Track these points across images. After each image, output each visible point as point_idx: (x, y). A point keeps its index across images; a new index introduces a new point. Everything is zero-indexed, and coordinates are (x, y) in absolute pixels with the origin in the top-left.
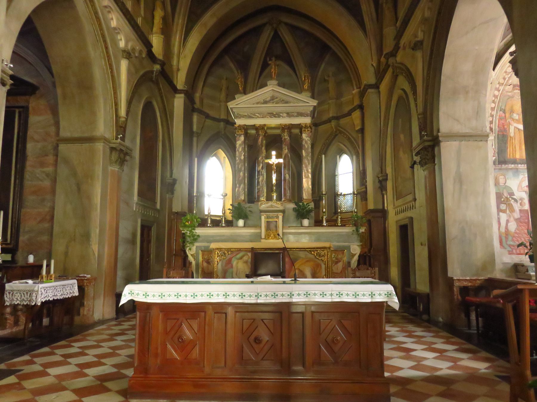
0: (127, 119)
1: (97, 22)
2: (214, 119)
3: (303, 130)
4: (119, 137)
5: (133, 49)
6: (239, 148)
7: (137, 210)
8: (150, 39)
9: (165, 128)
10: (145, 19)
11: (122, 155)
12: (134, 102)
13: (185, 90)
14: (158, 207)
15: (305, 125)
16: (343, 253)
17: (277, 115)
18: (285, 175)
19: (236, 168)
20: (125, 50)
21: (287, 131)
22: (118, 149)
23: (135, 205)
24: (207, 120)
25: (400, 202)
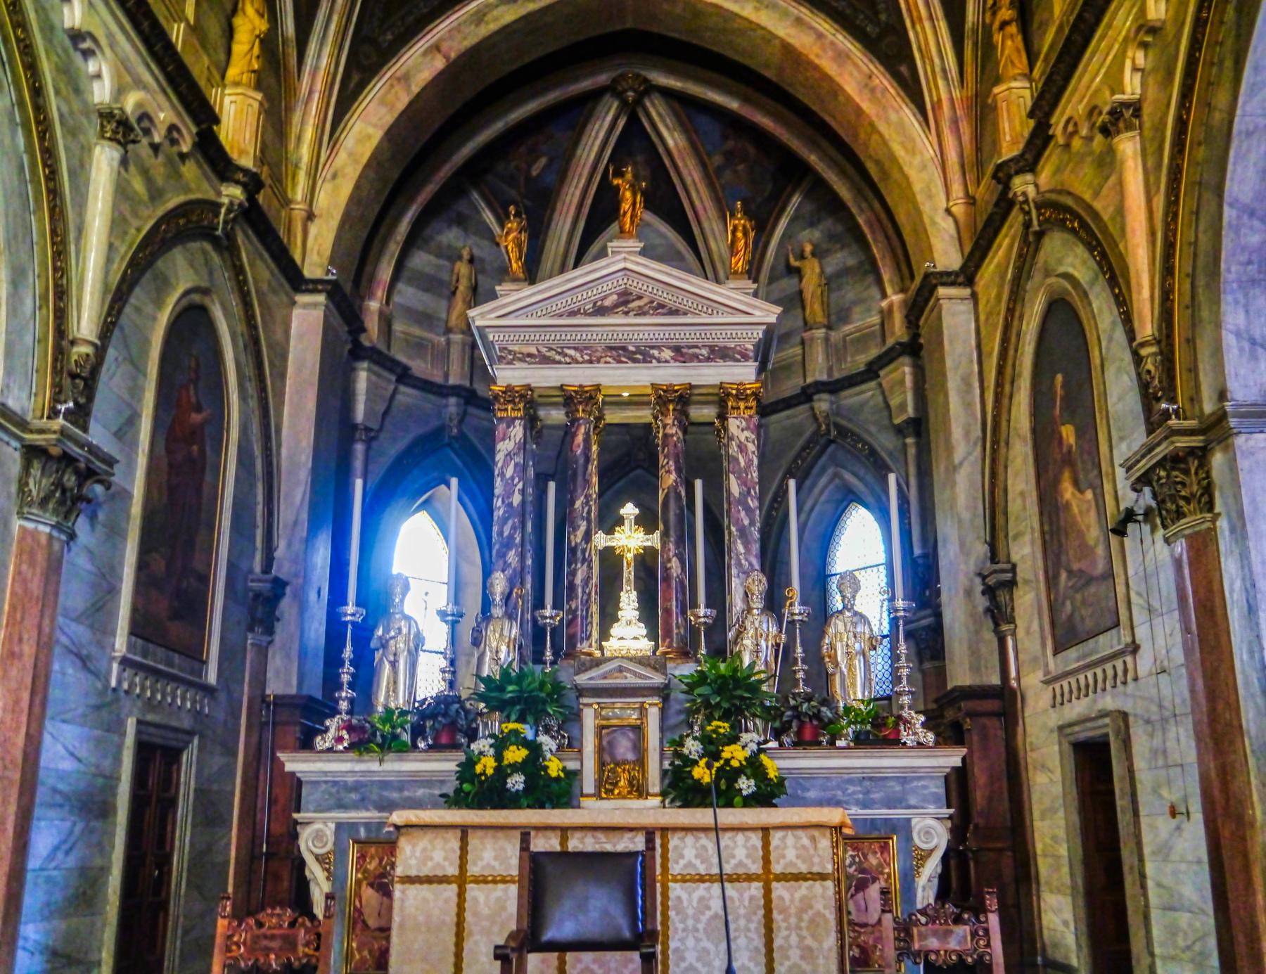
0: (101, 351)
2: (426, 386)
3: (730, 404)
4: (62, 408)
5: (145, 117)
6: (506, 464)
7: (125, 686)
9: (253, 403)
10: (196, 30)
11: (70, 480)
12: (138, 296)
13: (328, 282)
14: (212, 677)
15: (737, 389)
16: (884, 848)
17: (641, 355)
19: (495, 535)
21: (674, 410)
22: (55, 451)
23: (115, 666)
24: (402, 388)
25: (1072, 657)
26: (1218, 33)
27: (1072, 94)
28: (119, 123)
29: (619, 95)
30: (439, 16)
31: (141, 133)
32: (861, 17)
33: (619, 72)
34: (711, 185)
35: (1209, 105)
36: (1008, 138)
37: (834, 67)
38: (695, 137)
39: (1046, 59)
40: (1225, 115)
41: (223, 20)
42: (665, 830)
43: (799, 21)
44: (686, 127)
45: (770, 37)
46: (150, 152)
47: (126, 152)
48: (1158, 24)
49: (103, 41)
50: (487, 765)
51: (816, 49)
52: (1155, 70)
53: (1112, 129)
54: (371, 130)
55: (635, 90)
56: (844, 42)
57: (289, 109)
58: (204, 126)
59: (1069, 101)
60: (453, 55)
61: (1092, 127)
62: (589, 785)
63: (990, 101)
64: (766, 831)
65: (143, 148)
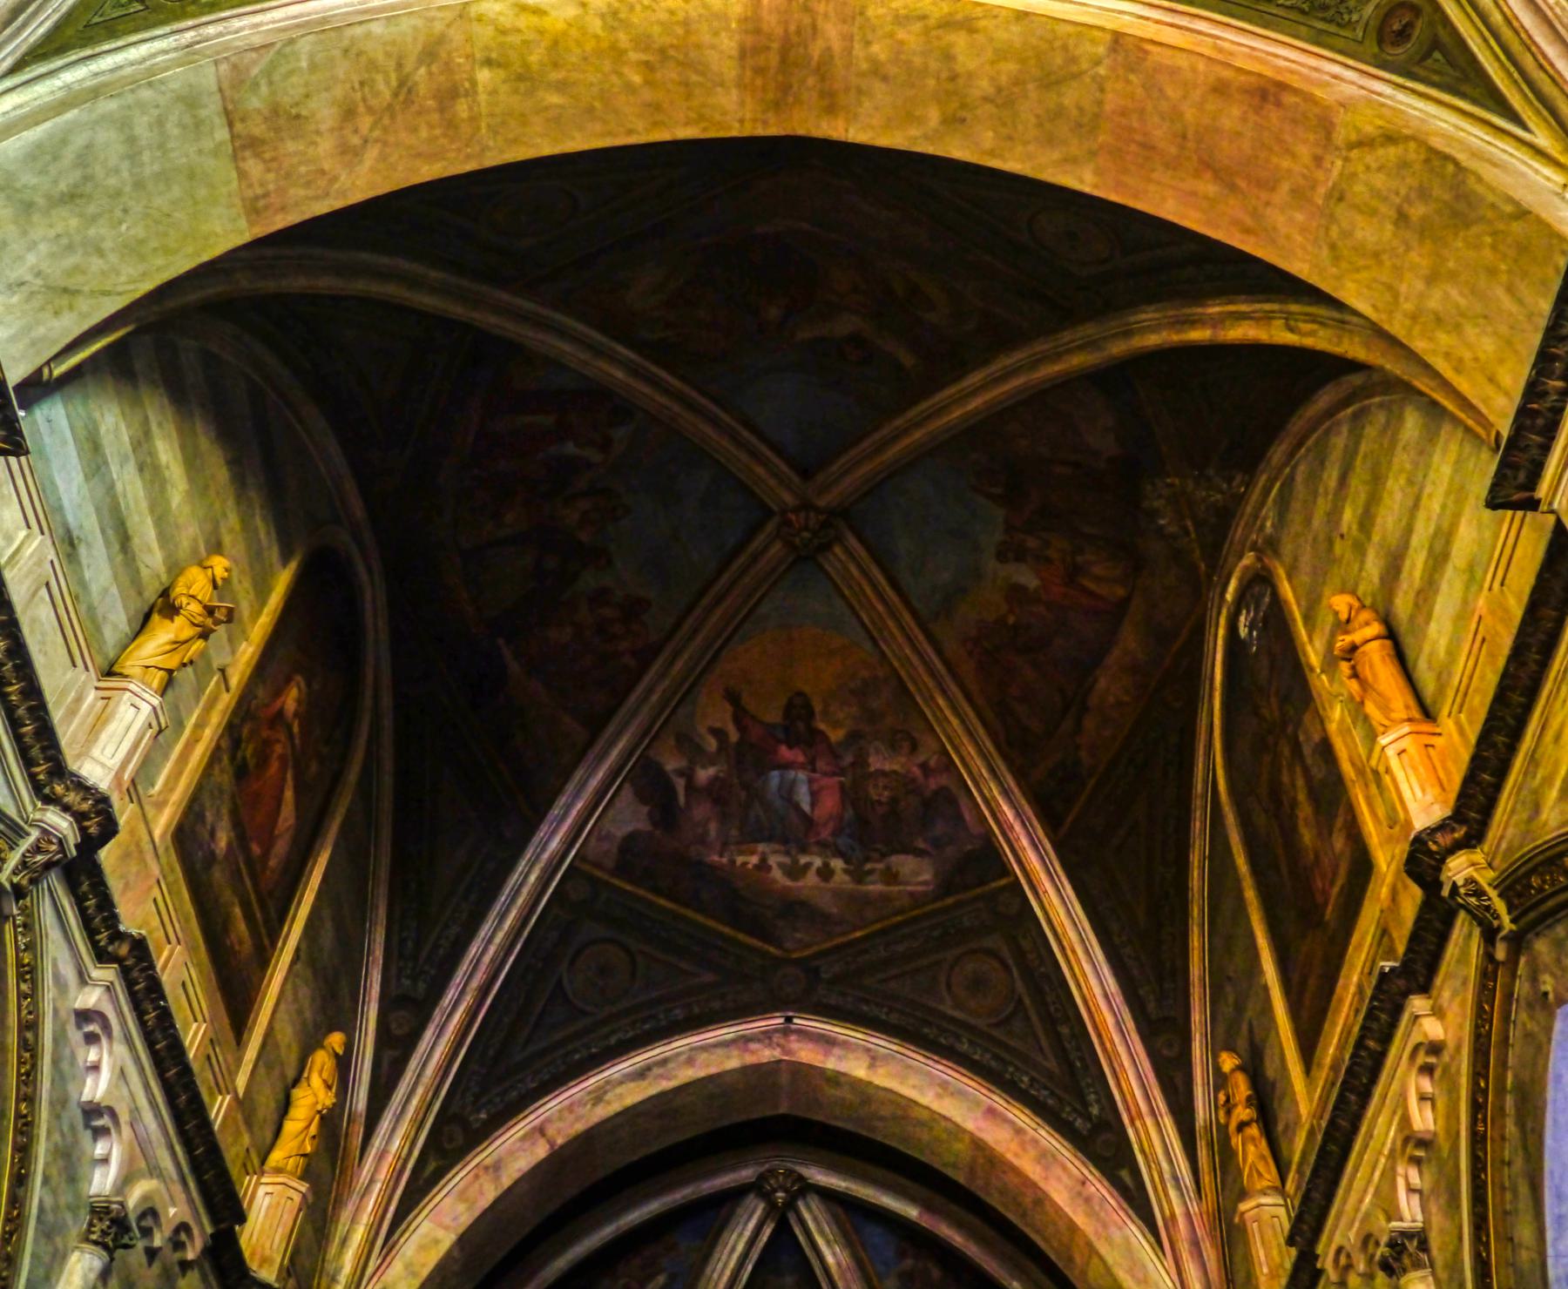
1: (21, 1063)
5: (150, 1213)
8: (167, 452)
10: (244, 1105)
20: (107, 1208)
26: (1503, 1149)
27: (1338, 1218)
28: (113, 1221)
29: (767, 1196)
30: (546, 1094)
31: (138, 1234)
32: (1068, 1109)
33: (767, 1166)
35: (1511, 1239)
36: (1265, 1270)
37: (1038, 1169)
38: (863, 1255)
39: (1300, 1171)
40: (1535, 1256)
41: (279, 1086)
43: (991, 1112)
44: (850, 1239)
45: (957, 1131)
46: (144, 1260)
47: (112, 1259)
48: (1428, 1137)
49: (124, 1117)
51: (1014, 1146)
52: (1434, 1190)
53: (1395, 1265)
54: (440, 1234)
55: (786, 1191)
57: (339, 1203)
58: (222, 1226)
59: (1336, 1226)
60: (560, 1141)
61: (1371, 1259)
63: (1237, 1220)
65: (136, 1256)
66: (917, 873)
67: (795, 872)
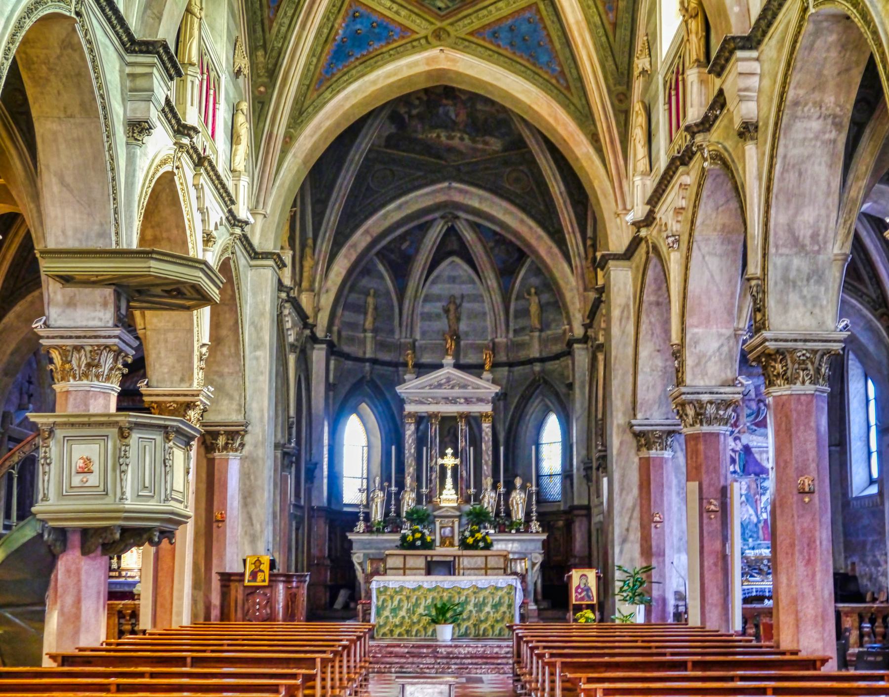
17: (454, 401)
18: (461, 471)
34: (488, 256)
42: (459, 556)
50: (410, 538)
56: (540, 231)
62: (438, 543)
64: (486, 557)
66: (495, 144)
67: (450, 138)
